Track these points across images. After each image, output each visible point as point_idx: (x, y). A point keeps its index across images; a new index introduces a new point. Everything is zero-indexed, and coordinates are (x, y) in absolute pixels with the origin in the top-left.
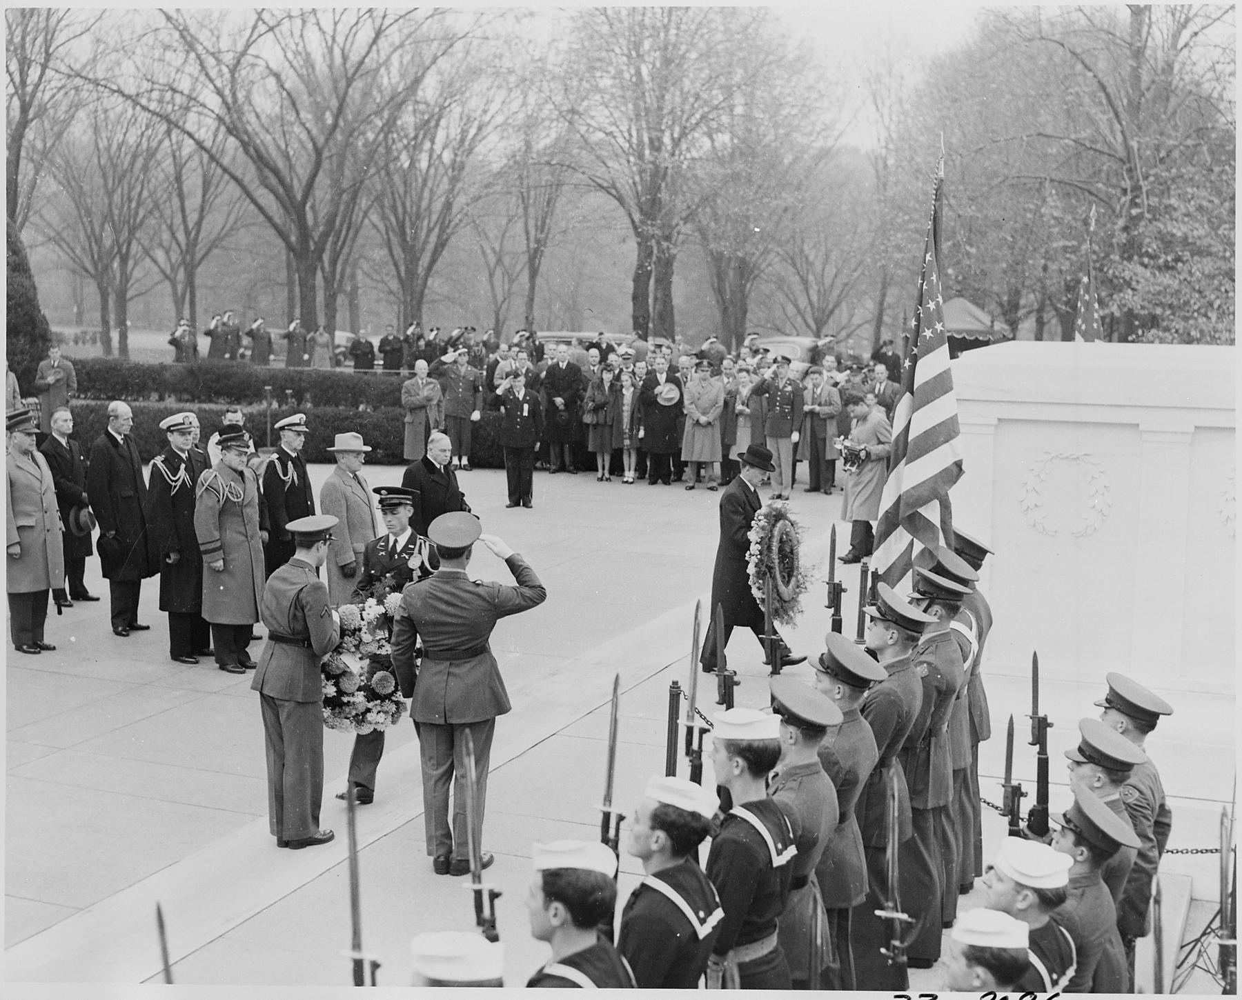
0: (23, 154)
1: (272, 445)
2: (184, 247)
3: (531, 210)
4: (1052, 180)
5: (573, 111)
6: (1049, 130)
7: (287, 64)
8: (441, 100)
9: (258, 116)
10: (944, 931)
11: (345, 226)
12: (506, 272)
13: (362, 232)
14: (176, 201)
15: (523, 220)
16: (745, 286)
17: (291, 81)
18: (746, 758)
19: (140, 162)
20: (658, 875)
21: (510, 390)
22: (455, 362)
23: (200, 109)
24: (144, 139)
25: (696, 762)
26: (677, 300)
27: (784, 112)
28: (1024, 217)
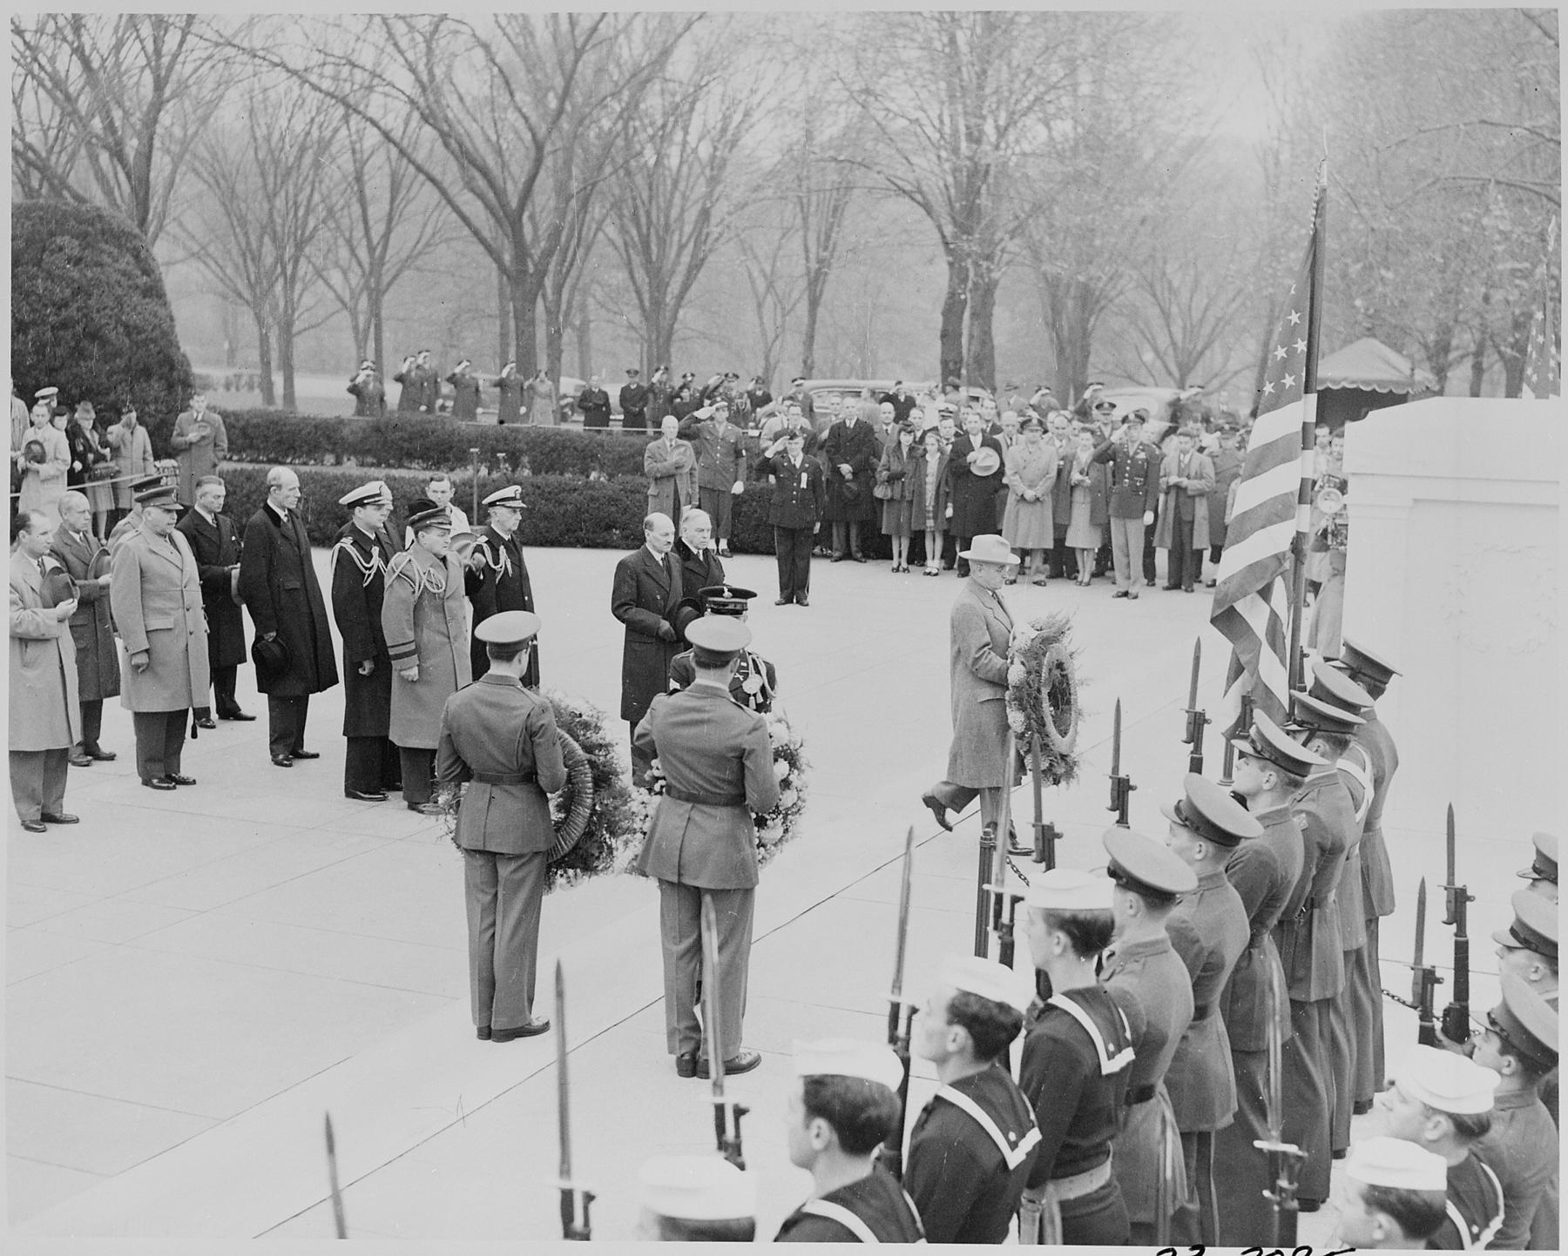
0: (157, 143)
1: (480, 523)
2: (367, 267)
3: (813, 221)
4: (1498, 183)
5: (867, 91)
6: (1496, 116)
7: (499, 31)
8: (697, 77)
9: (461, 99)
10: (1334, 1162)
11: (574, 241)
12: (779, 301)
13: (594, 250)
14: (356, 209)
15: (801, 233)
16: (1088, 320)
17: (505, 53)
18: (1069, 933)
19: (308, 159)
20: (956, 1085)
21: (783, 453)
22: (712, 418)
23: (387, 89)
24: (315, 126)
25: (1007, 938)
26: (999, 339)
27: (1144, 91)
28: (1459, 230)
